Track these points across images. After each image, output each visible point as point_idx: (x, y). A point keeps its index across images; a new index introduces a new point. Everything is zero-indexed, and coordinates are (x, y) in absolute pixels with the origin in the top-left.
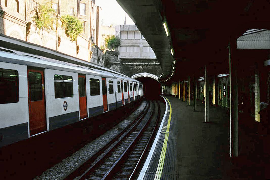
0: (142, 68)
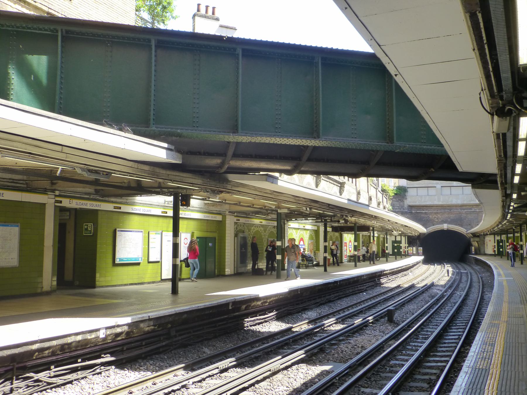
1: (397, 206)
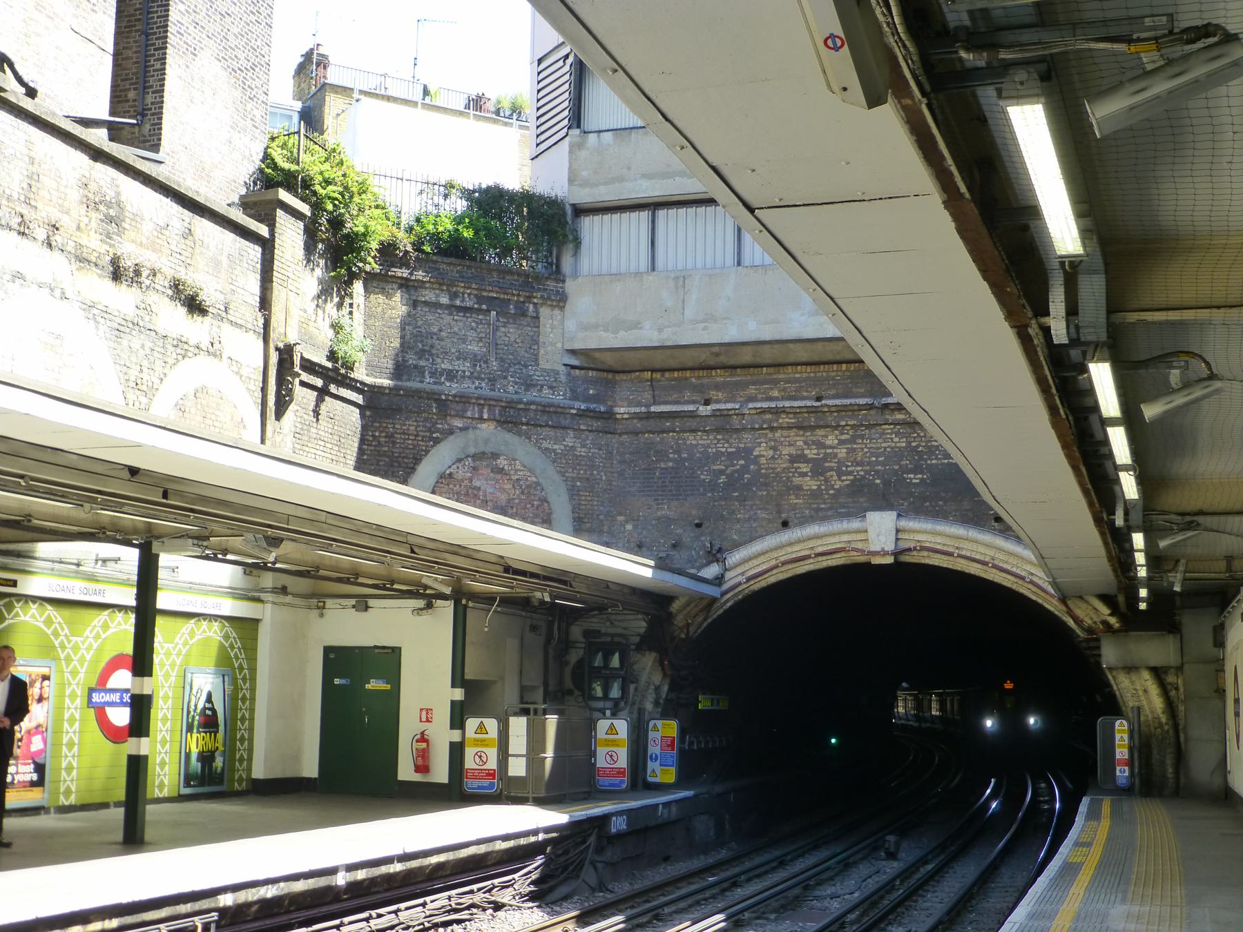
0: (842, 452)
1: (461, 356)
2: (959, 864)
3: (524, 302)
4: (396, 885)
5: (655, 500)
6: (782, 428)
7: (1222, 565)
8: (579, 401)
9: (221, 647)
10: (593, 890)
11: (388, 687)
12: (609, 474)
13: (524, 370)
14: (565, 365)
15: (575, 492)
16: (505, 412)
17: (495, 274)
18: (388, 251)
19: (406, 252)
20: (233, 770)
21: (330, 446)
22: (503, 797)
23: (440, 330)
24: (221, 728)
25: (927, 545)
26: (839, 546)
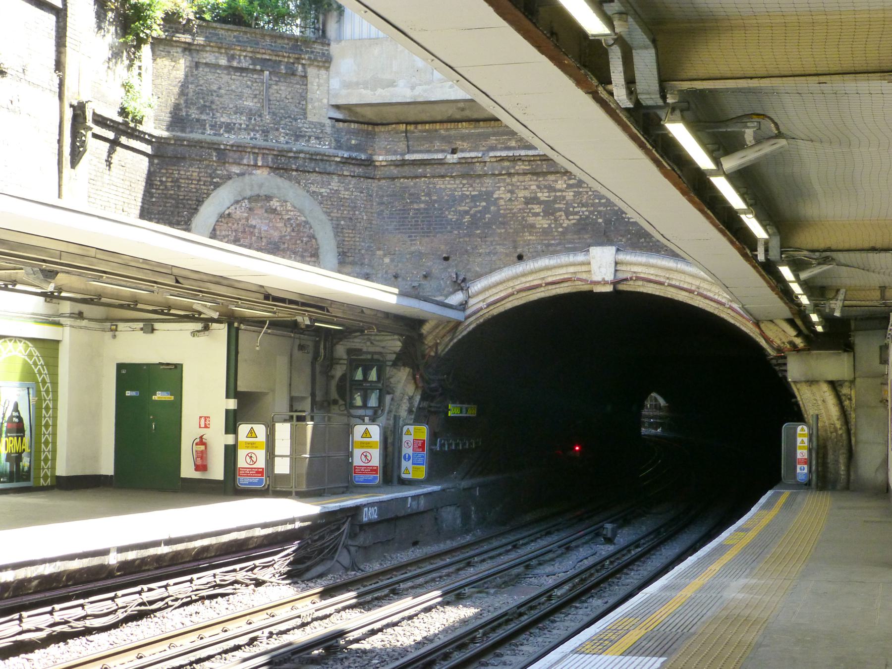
0: (570, 195)
1: (238, 111)
2: (667, 547)
3: (293, 63)
4: (165, 564)
5: (410, 237)
6: (518, 174)
7: (877, 294)
8: (342, 149)
9: (25, 364)
10: (346, 569)
11: (172, 398)
12: (369, 214)
13: (294, 123)
14: (330, 118)
15: (339, 230)
16: (277, 159)
17: (268, 39)
18: (171, 19)
19: (189, 20)
20: (39, 468)
21: (122, 190)
22: (270, 492)
23: (220, 88)
24: (27, 433)
25: (642, 275)
26: (566, 276)
